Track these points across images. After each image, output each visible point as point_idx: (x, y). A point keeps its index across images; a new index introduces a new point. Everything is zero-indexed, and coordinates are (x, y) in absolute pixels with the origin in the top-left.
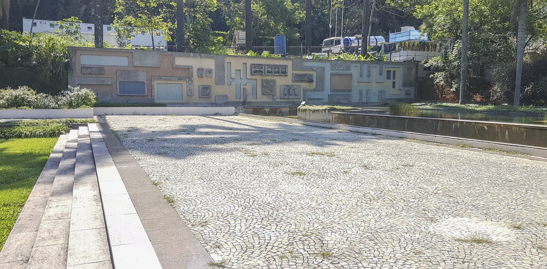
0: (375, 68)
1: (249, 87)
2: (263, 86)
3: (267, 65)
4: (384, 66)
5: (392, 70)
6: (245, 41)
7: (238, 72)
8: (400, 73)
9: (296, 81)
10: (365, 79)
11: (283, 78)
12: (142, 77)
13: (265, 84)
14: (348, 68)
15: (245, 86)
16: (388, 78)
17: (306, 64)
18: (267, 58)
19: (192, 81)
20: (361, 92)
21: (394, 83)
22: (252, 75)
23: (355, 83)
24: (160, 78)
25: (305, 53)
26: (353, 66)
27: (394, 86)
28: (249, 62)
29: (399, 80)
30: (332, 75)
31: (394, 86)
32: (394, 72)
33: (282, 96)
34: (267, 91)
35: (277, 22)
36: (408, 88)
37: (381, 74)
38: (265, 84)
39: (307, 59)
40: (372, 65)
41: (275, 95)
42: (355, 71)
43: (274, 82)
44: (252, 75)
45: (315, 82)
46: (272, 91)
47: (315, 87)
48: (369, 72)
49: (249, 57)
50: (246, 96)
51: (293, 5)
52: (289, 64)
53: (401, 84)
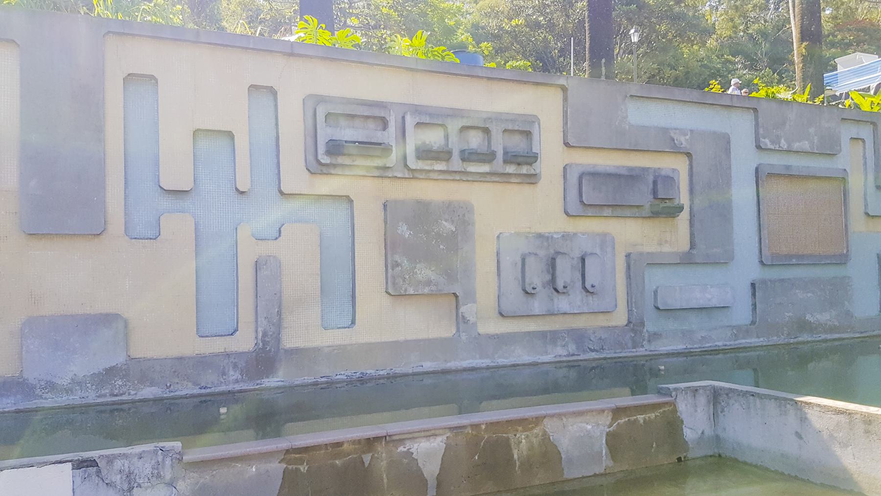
3: (417, 109)
9: (590, 209)
11: (516, 193)
30: (760, 176)
43: (461, 214)
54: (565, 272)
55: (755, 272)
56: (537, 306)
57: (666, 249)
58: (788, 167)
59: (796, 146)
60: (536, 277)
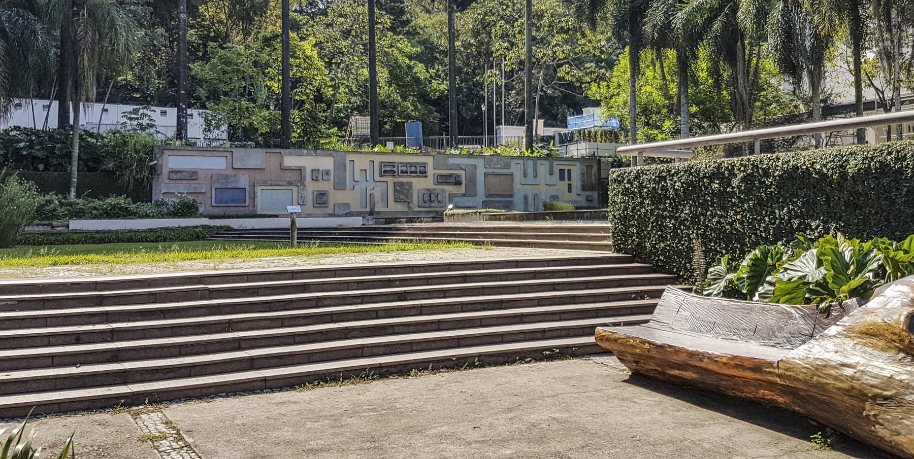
1: (378, 194)
12: (243, 181)
19: (305, 186)
24: (264, 183)
43: (410, 185)
56: (427, 205)
60: (427, 199)
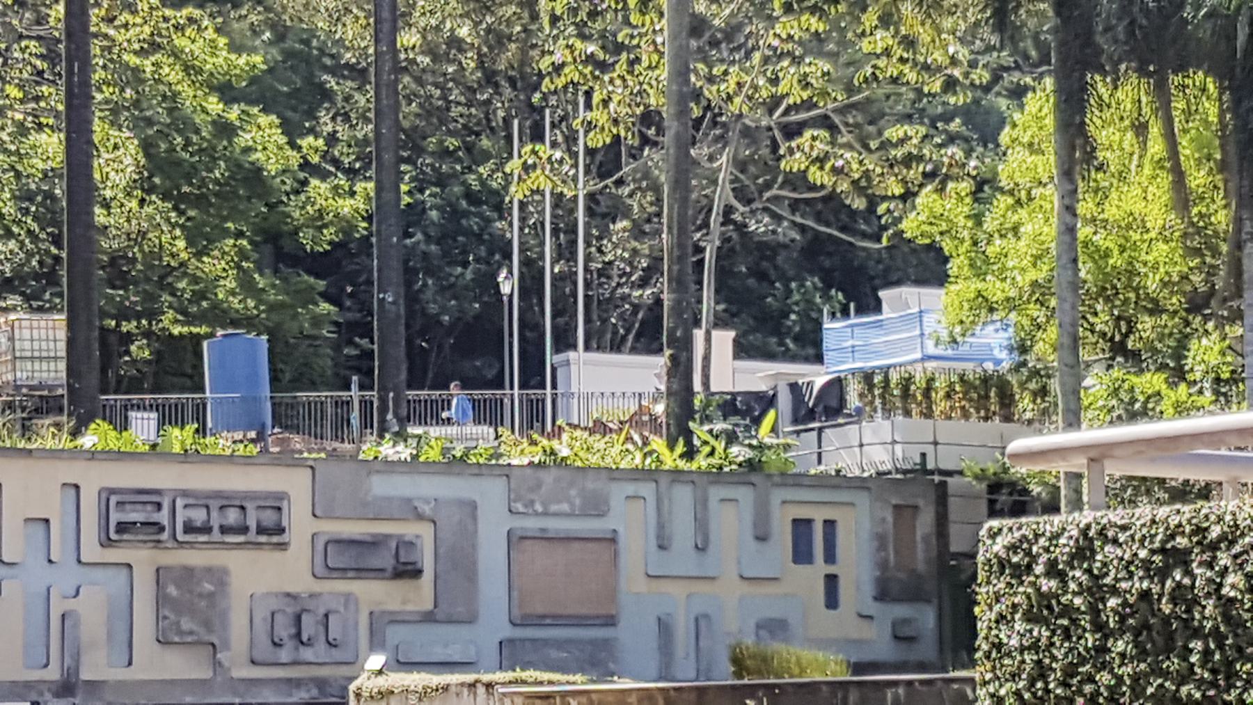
0: (729, 507)
1: (92, 612)
2: (161, 599)
3: (185, 493)
4: (778, 495)
5: (819, 516)
6: (62, 366)
7: (41, 527)
8: (858, 531)
9: (333, 572)
10: (682, 559)
11: (268, 558)
13: (172, 590)
14: (596, 507)
15: (71, 604)
16: (802, 554)
17: (381, 486)
18: (186, 456)
20: (664, 628)
21: (831, 580)
22: (107, 542)
23: (632, 581)
25: (374, 422)
26: (618, 492)
27: (832, 601)
28: (94, 479)
29: (857, 564)
30: (514, 540)
31: (832, 601)
32: (830, 524)
33: (264, 649)
34: (186, 624)
35: (201, 241)
36: (901, 611)
37: (762, 538)
38: (172, 590)
39: (386, 462)
40: (716, 493)
41: (227, 647)
42: (629, 518)
43: (220, 577)
44: (107, 542)
45: (428, 575)
46: (208, 625)
47: (429, 606)
48: (702, 524)
49: (92, 455)
50: (73, 654)
51: (293, 145)
52: (294, 485)
53: (869, 590)
54: (309, 626)
55: (508, 632)
56: (284, 655)
57: (410, 607)
58: (543, 530)
59: (554, 508)
